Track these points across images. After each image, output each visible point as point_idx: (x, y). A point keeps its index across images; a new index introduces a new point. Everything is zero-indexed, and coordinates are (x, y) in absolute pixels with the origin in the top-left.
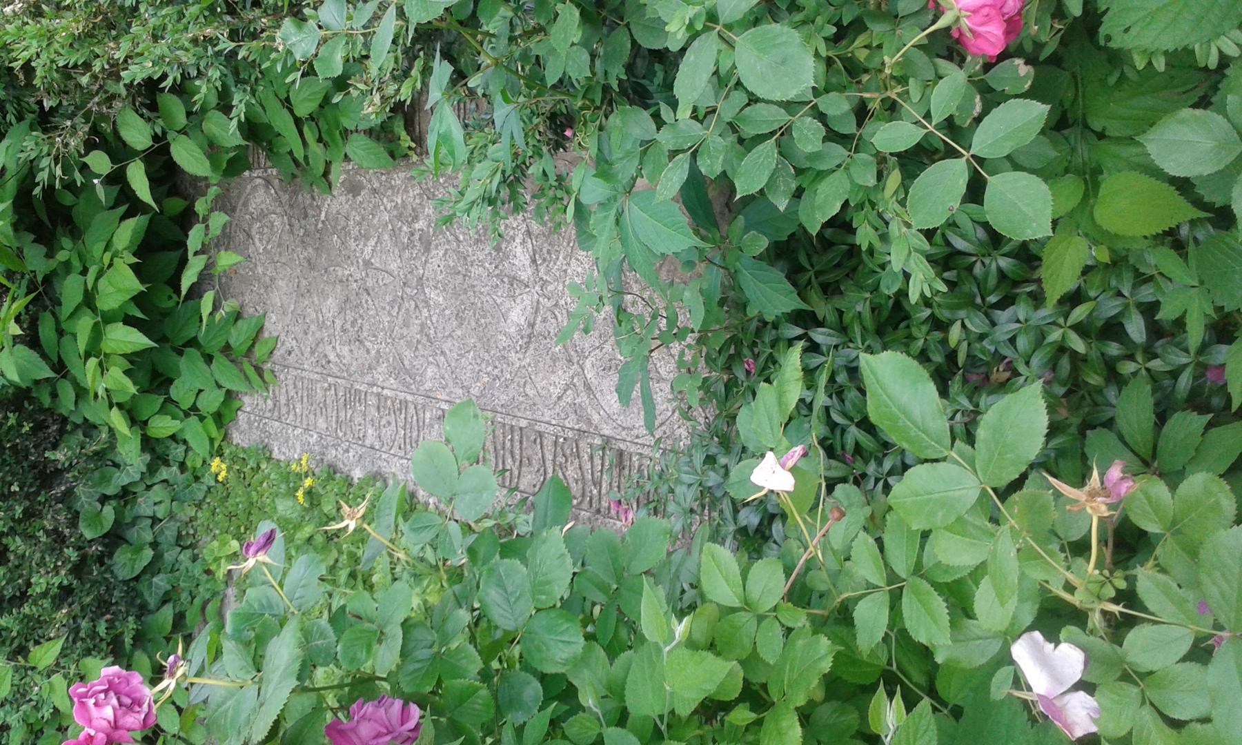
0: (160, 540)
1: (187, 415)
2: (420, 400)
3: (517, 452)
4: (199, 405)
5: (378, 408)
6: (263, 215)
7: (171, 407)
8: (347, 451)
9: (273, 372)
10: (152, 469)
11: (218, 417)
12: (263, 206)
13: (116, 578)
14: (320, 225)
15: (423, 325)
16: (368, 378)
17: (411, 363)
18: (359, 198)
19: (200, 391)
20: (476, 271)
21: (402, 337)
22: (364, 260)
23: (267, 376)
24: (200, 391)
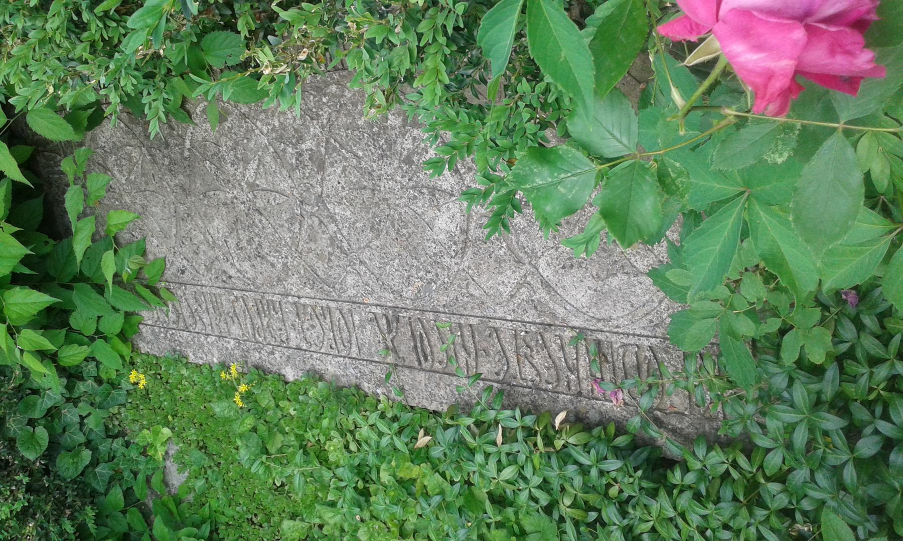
0: (92, 437)
1: (92, 339)
2: (346, 307)
3: (470, 345)
4: (101, 329)
5: (298, 315)
6: (116, 148)
7: (75, 336)
8: (272, 353)
9: (168, 289)
10: (70, 387)
11: (122, 336)
12: (114, 139)
13: (64, 480)
14: (187, 154)
15: (332, 240)
16: (279, 289)
17: (326, 273)
18: (227, 124)
19: (99, 317)
20: (384, 185)
21: (310, 250)
22: (248, 183)
23: (163, 293)
24: (99, 317)
